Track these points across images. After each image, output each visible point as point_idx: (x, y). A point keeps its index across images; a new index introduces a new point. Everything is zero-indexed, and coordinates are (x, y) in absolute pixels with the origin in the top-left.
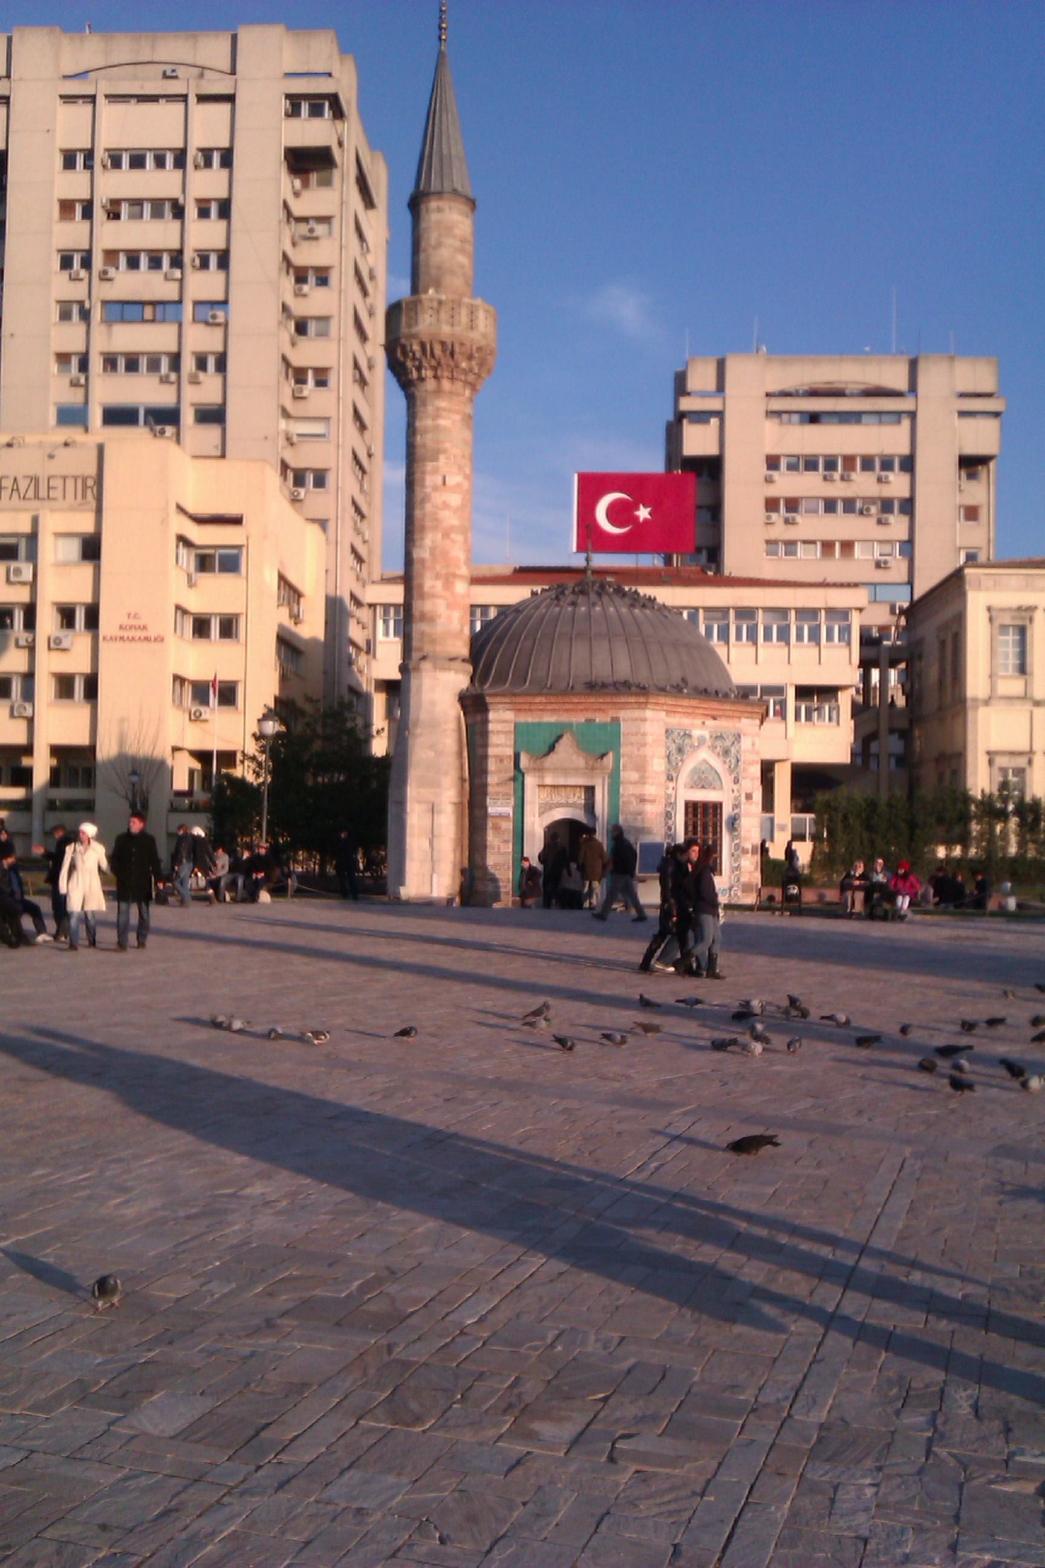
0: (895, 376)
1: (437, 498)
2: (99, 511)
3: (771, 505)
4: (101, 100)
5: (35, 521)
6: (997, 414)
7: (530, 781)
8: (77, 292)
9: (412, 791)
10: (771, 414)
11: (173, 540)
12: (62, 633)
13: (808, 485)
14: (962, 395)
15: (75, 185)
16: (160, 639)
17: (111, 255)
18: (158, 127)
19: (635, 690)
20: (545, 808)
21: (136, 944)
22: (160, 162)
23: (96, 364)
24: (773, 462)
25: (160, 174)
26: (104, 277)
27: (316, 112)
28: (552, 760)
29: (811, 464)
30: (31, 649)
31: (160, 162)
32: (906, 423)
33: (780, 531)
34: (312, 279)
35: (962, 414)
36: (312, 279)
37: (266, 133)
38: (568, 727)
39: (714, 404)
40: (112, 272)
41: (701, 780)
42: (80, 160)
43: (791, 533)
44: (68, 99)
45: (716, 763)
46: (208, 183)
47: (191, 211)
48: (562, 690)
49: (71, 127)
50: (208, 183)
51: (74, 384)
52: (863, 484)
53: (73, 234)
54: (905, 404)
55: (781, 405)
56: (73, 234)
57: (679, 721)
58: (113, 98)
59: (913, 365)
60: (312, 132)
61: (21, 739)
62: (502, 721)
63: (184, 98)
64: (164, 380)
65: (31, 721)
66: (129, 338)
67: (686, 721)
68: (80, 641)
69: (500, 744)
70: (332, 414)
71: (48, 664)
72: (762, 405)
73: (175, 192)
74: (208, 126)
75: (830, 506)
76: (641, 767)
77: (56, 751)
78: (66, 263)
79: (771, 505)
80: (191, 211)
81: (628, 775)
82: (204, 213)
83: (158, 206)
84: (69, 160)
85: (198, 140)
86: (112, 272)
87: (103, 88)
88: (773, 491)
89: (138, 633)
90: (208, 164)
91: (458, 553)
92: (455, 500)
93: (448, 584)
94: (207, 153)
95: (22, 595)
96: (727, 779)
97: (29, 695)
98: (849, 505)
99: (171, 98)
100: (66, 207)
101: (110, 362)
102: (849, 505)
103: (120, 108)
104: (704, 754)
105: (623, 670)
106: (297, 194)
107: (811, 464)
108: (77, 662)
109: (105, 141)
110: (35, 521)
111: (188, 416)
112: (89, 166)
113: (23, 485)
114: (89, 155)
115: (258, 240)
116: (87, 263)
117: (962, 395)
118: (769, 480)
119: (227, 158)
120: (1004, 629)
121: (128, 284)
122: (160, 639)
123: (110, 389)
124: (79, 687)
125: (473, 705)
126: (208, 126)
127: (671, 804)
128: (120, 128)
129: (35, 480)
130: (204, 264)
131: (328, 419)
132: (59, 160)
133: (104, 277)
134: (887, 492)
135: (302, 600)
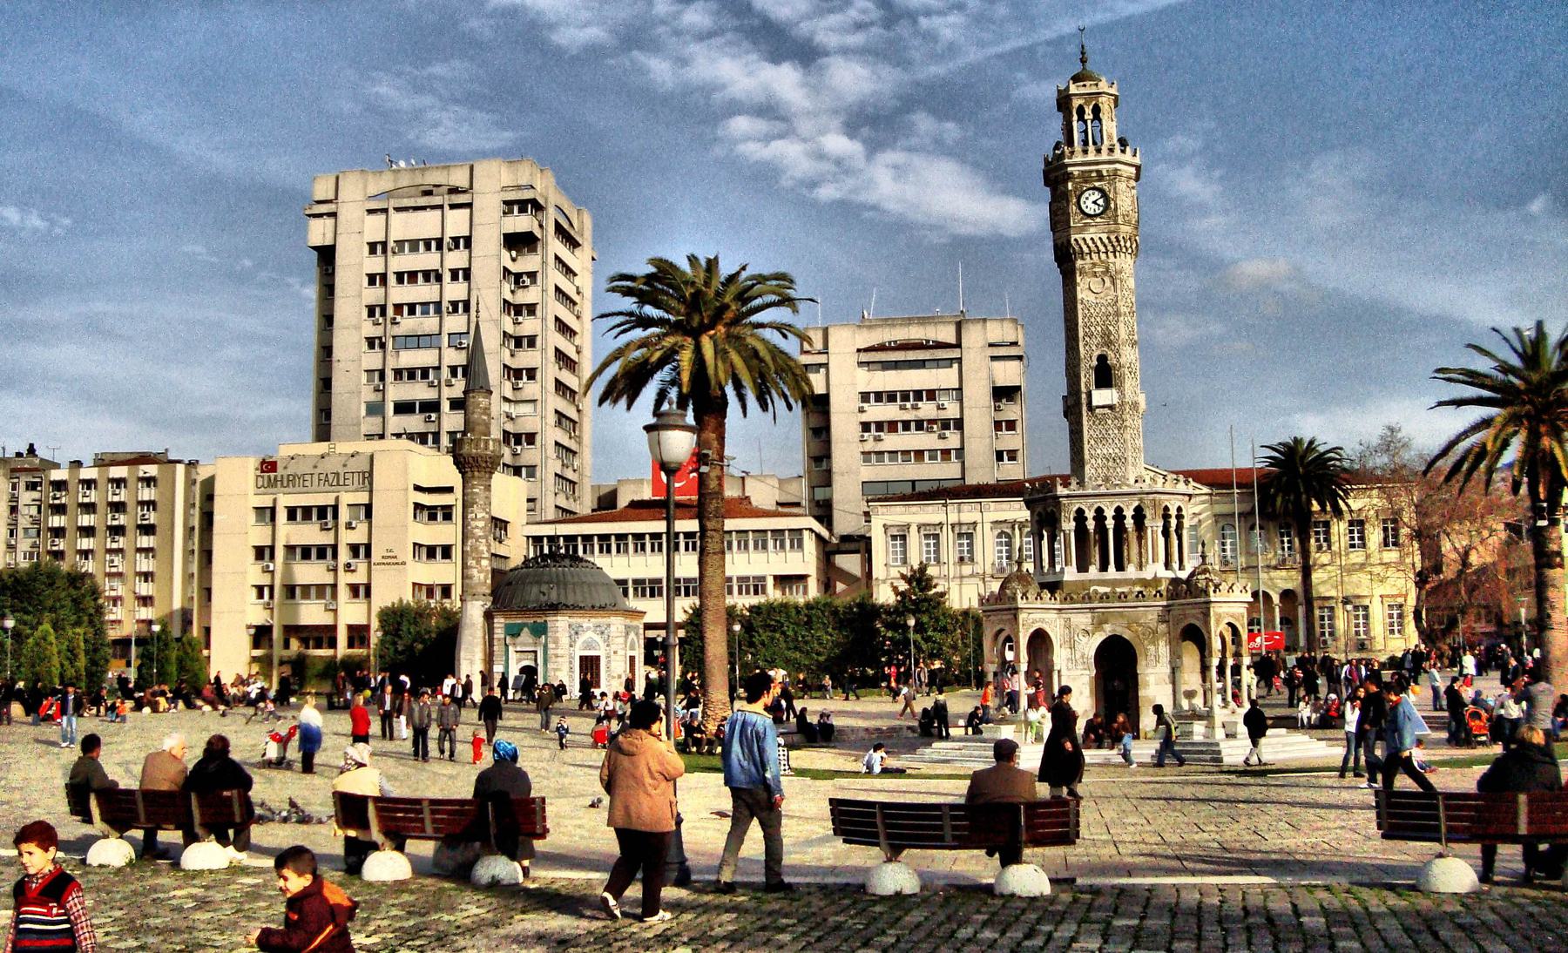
0: (947, 334)
1: (474, 524)
2: (371, 492)
3: (866, 427)
4: (391, 211)
5: (337, 499)
6: (1020, 358)
7: (511, 649)
8: (376, 332)
9: (462, 654)
10: (861, 364)
11: (412, 507)
12: (353, 561)
13: (889, 412)
14: (991, 345)
15: (375, 265)
16: (404, 563)
17: (398, 308)
18: (425, 225)
19: (555, 608)
20: (519, 661)
21: (379, 733)
22: (428, 247)
23: (390, 376)
24: (865, 397)
25: (428, 255)
26: (394, 322)
27: (523, 210)
28: (520, 639)
29: (892, 397)
30: (335, 570)
31: (428, 247)
32: (956, 366)
33: (870, 446)
34: (525, 312)
35: (994, 358)
36: (525, 312)
37: (491, 224)
38: (525, 625)
39: (822, 359)
40: (399, 318)
41: (588, 646)
42: (379, 248)
43: (880, 447)
44: (370, 212)
45: (598, 638)
46: (456, 259)
47: (447, 277)
48: (524, 610)
49: (374, 228)
50: (456, 259)
51: (377, 390)
52: (927, 410)
53: (374, 295)
54: (955, 354)
55: (877, 357)
56: (374, 295)
57: (576, 620)
58: (398, 209)
59: (959, 326)
60: (521, 223)
61: (330, 622)
62: (499, 622)
63: (441, 207)
64: (431, 385)
65: (335, 611)
66: (410, 359)
67: (579, 620)
68: (361, 566)
69: (499, 633)
70: (538, 397)
71: (344, 579)
72: (854, 358)
73: (436, 266)
74: (457, 223)
75: (906, 425)
76: (556, 642)
77: (351, 628)
78: (371, 313)
79: (866, 427)
80: (447, 277)
81: (551, 646)
82: (455, 277)
83: (427, 275)
84: (373, 247)
85: (451, 232)
86: (399, 318)
87: (393, 203)
88: (865, 418)
89: (391, 560)
90: (457, 247)
91: (483, 548)
92: (481, 524)
93: (478, 562)
94: (456, 240)
95: (432, 428)
96: (603, 645)
97: (334, 596)
98: (920, 425)
99: (433, 207)
100: (372, 279)
101: (398, 373)
102: (920, 425)
103: (403, 215)
104: (590, 634)
105: (554, 597)
106: (514, 260)
107: (892, 397)
108: (359, 578)
109: (395, 235)
110: (337, 499)
111: (445, 406)
112: (384, 251)
113: (331, 477)
114: (384, 244)
115: (489, 292)
116: (383, 314)
117: (991, 345)
118: (861, 410)
119: (468, 241)
120: (894, 537)
121: (408, 324)
122: (404, 563)
123: (398, 392)
124: (362, 591)
125: (489, 616)
126: (457, 223)
127: (571, 657)
128: (405, 226)
129: (337, 474)
130: (455, 310)
131: (534, 401)
132: (366, 249)
133: (394, 322)
134: (943, 415)
135: (509, 527)
